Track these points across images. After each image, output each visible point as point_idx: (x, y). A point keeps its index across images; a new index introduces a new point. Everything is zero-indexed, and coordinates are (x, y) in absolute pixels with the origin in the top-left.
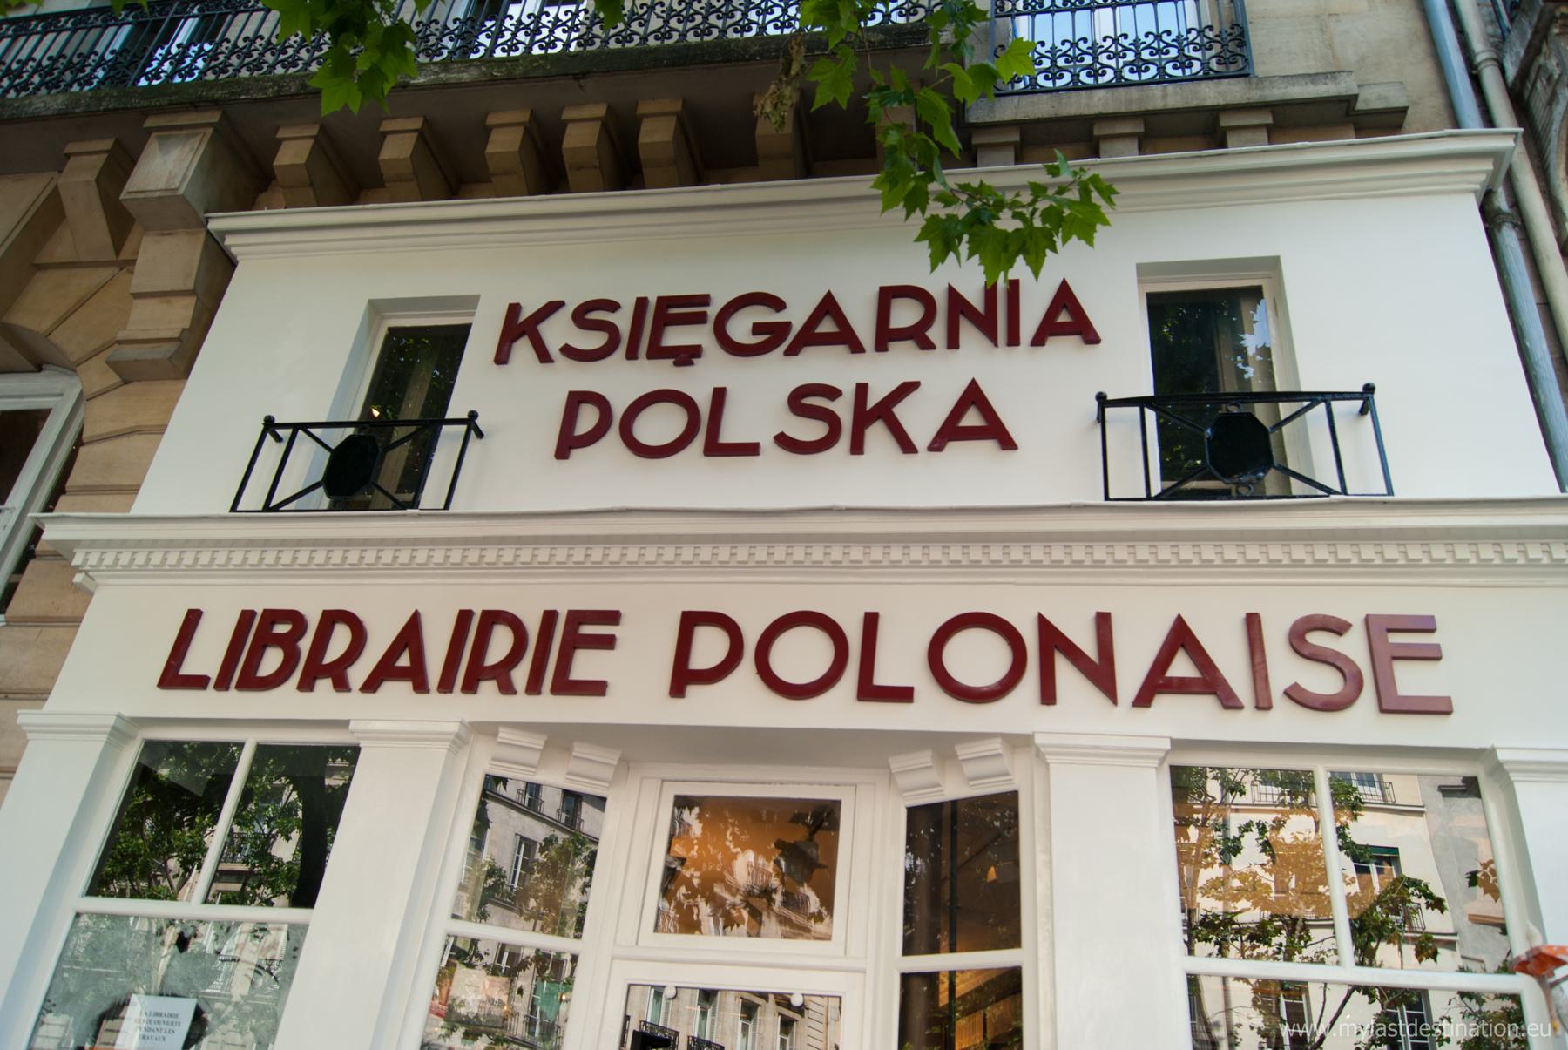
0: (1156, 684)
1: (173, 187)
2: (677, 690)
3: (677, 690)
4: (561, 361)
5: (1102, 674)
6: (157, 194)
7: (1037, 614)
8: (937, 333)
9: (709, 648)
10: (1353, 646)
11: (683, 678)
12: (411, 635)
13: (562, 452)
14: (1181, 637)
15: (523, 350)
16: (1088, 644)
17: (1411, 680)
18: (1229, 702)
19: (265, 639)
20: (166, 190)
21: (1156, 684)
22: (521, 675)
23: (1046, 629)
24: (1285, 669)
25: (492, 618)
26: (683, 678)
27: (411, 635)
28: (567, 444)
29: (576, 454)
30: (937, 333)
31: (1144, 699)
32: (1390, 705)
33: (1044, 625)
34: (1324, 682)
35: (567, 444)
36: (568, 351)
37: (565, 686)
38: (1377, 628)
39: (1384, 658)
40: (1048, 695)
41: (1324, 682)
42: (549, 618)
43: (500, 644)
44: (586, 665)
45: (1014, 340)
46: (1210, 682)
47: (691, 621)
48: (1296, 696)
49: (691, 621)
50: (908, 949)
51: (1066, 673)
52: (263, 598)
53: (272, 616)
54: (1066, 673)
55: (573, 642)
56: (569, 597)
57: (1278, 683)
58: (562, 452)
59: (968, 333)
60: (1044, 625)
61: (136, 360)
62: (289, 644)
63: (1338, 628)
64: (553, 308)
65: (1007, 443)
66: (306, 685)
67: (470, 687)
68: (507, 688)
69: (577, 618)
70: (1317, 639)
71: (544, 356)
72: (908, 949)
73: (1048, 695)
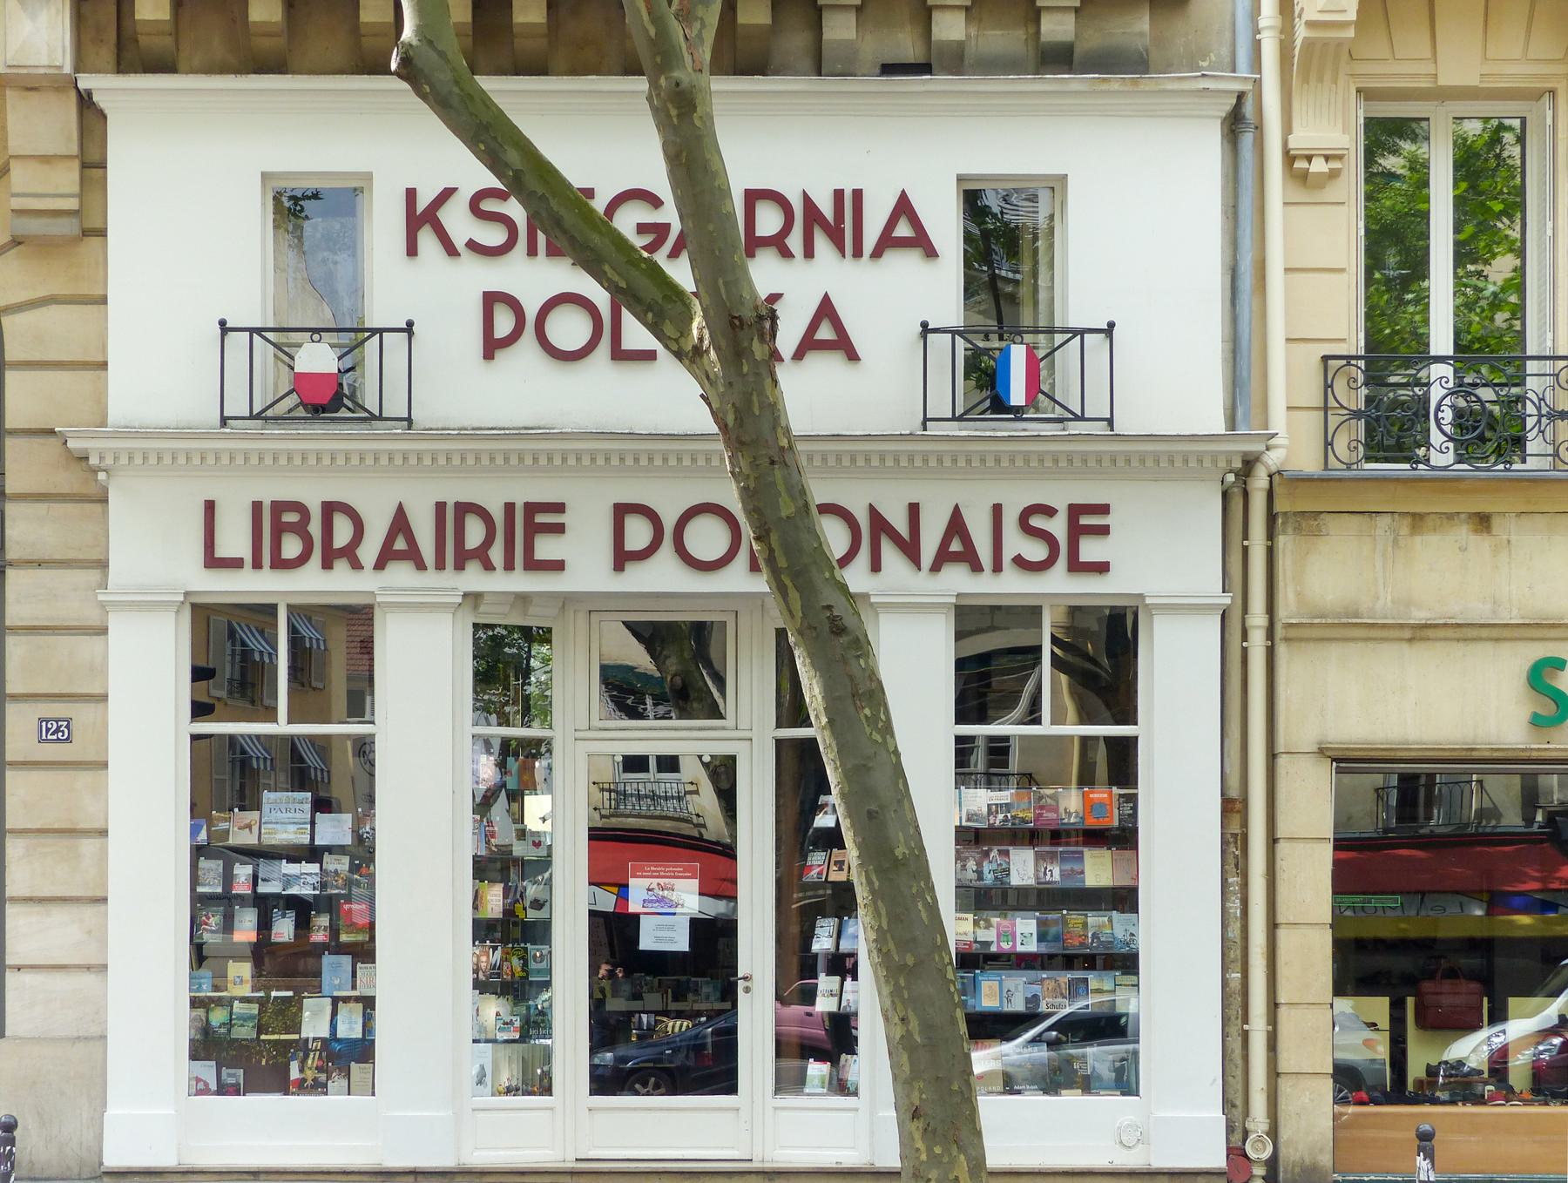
0: (943, 557)
1: (58, 64)
2: (619, 566)
3: (619, 566)
4: (468, 258)
5: (910, 549)
6: (42, 71)
7: (868, 504)
8: (795, 241)
9: (638, 534)
10: (1058, 527)
11: (622, 558)
12: (400, 523)
13: (489, 354)
14: (903, 207)
15: (427, 240)
16: (902, 527)
17: (1090, 550)
18: (977, 567)
19: (279, 530)
20: (50, 67)
21: (943, 557)
22: (496, 554)
23: (874, 515)
24: (1016, 543)
25: (463, 509)
26: (622, 558)
27: (400, 523)
28: (492, 347)
29: (499, 354)
30: (795, 241)
31: (936, 568)
32: (1077, 566)
33: (874, 513)
34: (1036, 551)
35: (492, 347)
36: (472, 245)
37: (533, 565)
38: (1075, 511)
39: (1076, 532)
40: (876, 566)
41: (1036, 551)
42: (510, 508)
43: (475, 533)
44: (546, 548)
45: (858, 253)
46: (969, 558)
47: (622, 511)
48: (1020, 562)
49: (622, 511)
50: (779, 726)
51: (889, 552)
52: (272, 490)
53: (279, 507)
54: (889, 552)
55: (533, 530)
56: (525, 491)
57: (1008, 556)
58: (489, 354)
59: (821, 243)
60: (874, 513)
61: (44, 235)
62: (301, 529)
63: (1049, 512)
64: (447, 194)
65: (853, 356)
66: (327, 565)
67: (460, 566)
68: (488, 566)
69: (532, 509)
70: (1037, 522)
71: (451, 251)
72: (779, 726)
73: (876, 566)
